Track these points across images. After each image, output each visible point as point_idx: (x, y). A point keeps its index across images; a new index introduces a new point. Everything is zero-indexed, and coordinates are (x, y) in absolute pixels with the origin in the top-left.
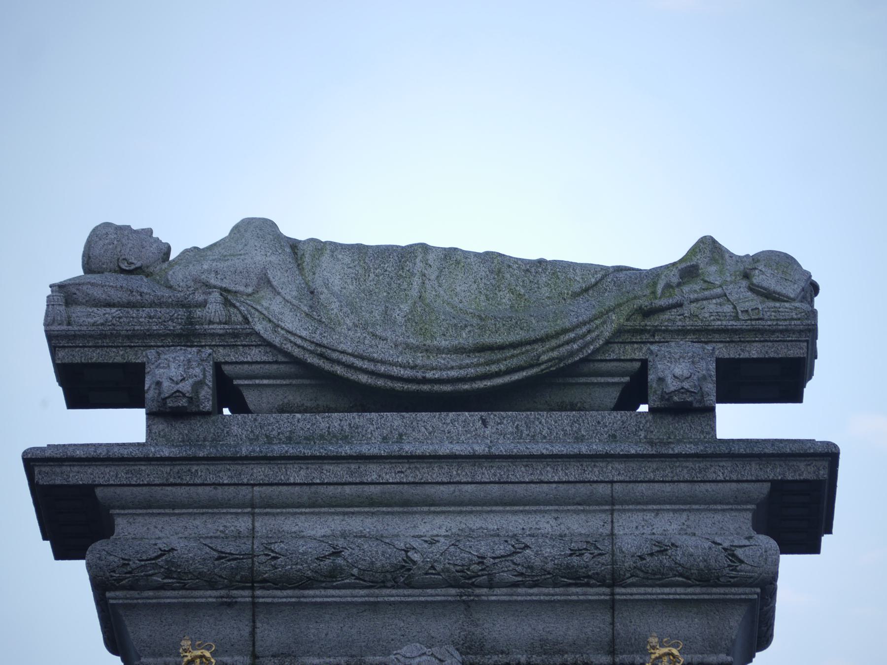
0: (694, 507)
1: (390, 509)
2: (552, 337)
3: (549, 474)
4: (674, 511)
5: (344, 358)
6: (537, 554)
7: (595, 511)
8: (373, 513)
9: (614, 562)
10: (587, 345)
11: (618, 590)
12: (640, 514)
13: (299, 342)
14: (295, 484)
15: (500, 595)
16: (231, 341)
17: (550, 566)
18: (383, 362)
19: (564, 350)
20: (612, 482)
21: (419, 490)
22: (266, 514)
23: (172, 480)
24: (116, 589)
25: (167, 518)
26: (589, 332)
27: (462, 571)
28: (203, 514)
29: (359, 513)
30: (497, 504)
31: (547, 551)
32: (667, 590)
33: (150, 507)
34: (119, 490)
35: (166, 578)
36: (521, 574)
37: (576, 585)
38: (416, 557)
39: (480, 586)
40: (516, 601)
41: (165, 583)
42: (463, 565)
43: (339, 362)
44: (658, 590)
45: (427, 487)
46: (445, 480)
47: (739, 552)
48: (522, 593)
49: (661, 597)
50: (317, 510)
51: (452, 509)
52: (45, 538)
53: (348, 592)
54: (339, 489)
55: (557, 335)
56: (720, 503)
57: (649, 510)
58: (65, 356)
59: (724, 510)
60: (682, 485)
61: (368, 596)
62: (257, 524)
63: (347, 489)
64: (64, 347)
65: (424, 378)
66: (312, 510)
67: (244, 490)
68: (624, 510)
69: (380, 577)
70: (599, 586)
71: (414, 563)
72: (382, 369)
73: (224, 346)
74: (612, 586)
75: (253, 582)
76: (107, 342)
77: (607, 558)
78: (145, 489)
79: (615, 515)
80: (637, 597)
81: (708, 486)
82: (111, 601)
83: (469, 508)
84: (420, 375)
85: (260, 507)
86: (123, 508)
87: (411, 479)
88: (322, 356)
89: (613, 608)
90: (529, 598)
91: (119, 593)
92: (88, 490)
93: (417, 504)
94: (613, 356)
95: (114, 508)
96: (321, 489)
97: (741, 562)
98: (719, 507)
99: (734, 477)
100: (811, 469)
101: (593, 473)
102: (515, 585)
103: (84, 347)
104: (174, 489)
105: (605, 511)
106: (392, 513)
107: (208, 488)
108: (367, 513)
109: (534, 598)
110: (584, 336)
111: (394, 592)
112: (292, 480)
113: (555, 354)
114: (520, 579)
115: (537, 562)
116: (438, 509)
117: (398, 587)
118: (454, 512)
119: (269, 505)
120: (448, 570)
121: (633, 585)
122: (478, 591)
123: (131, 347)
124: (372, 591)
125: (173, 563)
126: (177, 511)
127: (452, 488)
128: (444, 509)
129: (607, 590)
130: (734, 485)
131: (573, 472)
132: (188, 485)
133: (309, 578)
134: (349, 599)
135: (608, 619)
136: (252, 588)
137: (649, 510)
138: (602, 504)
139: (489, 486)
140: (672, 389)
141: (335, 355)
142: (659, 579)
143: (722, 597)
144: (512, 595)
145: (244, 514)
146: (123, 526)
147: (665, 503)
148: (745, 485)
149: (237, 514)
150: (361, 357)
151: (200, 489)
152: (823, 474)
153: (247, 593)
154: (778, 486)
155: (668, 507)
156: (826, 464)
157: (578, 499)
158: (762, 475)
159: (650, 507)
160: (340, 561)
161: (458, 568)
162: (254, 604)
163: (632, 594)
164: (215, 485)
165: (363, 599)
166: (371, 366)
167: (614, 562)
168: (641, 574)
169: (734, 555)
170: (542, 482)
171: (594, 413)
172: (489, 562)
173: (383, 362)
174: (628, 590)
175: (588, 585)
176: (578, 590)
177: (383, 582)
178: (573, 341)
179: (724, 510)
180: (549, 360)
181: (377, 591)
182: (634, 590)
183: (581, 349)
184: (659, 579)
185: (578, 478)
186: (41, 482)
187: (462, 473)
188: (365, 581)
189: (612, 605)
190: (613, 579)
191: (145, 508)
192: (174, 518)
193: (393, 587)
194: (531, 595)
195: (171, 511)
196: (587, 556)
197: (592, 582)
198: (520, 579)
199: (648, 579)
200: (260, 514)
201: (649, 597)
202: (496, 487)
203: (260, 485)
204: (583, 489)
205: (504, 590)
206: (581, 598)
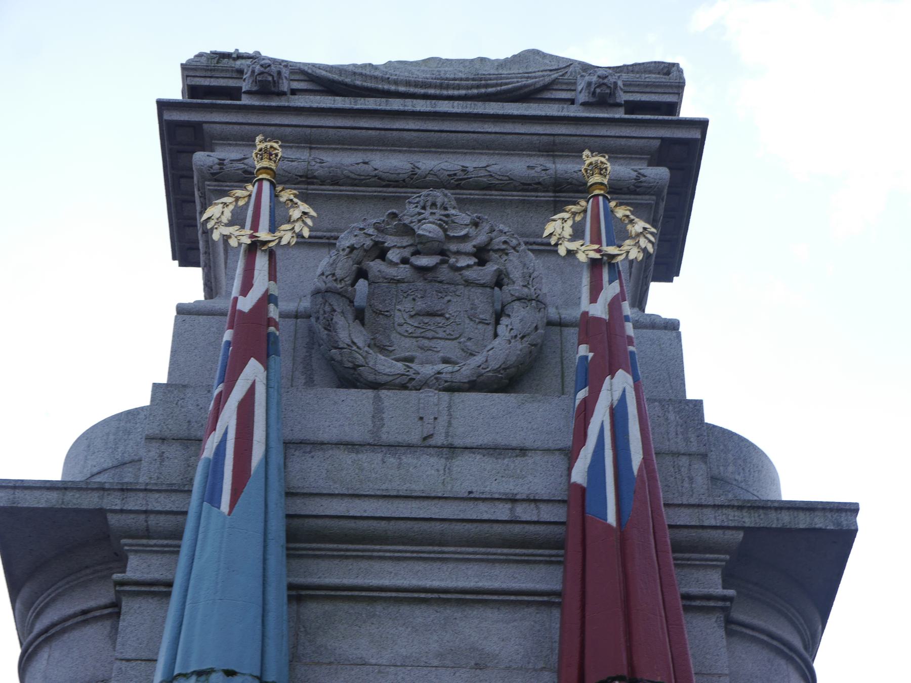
154: (666, 142)
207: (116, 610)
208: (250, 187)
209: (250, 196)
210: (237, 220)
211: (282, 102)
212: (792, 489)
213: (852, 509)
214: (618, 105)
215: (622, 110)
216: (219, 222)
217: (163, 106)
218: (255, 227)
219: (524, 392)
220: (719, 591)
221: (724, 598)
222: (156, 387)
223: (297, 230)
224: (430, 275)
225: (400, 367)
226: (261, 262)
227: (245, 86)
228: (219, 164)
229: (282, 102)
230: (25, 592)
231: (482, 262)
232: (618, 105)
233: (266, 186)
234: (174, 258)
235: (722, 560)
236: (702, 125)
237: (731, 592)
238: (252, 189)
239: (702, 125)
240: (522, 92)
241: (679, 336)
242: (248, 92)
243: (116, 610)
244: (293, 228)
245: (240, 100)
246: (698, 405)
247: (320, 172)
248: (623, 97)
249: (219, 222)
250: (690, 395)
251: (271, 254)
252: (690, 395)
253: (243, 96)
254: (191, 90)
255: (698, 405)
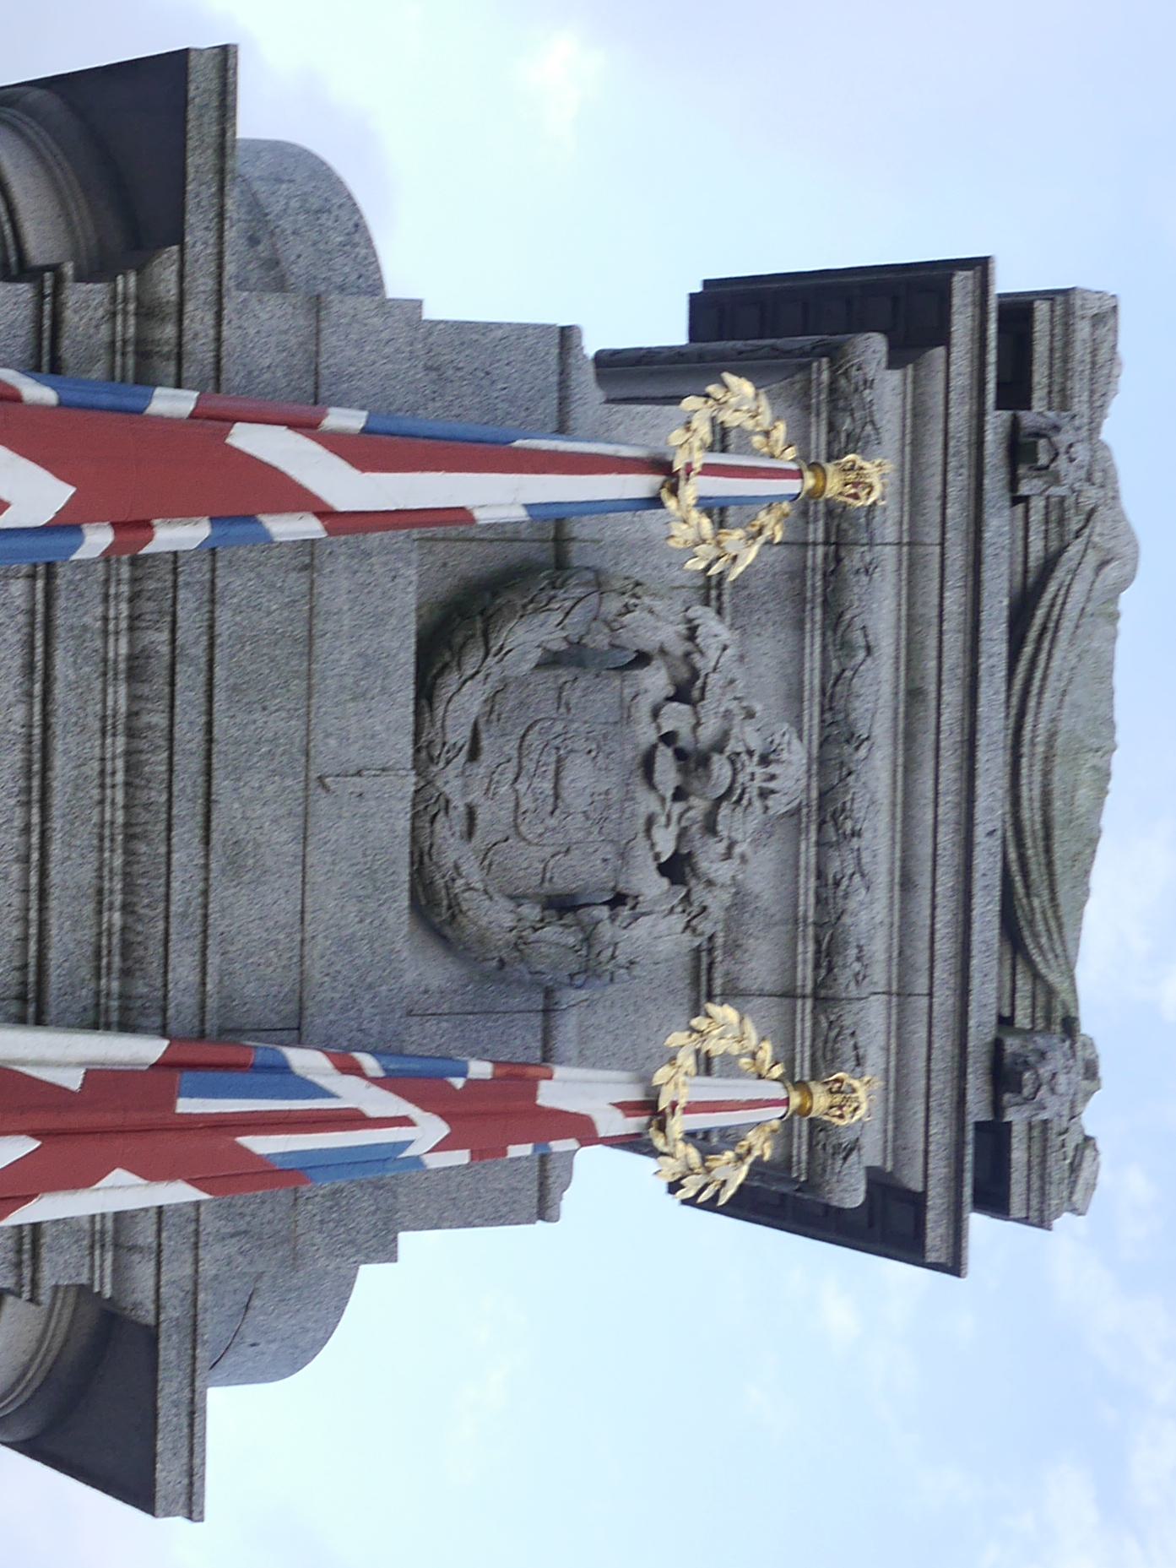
0: (892, 1095)
1: (901, 716)
2: (1055, 912)
3: (944, 917)
4: (887, 1070)
5: (1043, 656)
6: (862, 904)
7: (889, 971)
8: (896, 694)
9: (850, 1000)
10: (1042, 953)
11: (809, 1003)
12: (883, 1028)
13: (1060, 600)
14: (942, 598)
15: (808, 853)
16: (1054, 517)
17: (847, 920)
18: (1039, 703)
19: (1041, 927)
20: (931, 995)
21: (929, 755)
22: (900, 561)
23: (952, 443)
24: (833, 372)
25: (898, 437)
26: (1056, 956)
27: (843, 810)
28: (902, 480)
29: (898, 678)
30: (904, 851)
31: (864, 916)
32: (807, 1065)
33: (915, 416)
34: (941, 376)
35: (848, 436)
36: (837, 884)
37: (818, 952)
38: (863, 752)
39: (820, 830)
40: (797, 876)
41: (838, 433)
42: (852, 810)
43: (1037, 651)
44: (807, 1054)
45: (932, 763)
46: (940, 787)
47: (854, 1157)
48: (808, 884)
49: (798, 1056)
50: (903, 623)
51: (900, 794)
52: (707, 283)
53: (817, 664)
54: (934, 653)
55: (1058, 918)
56: (896, 1128)
57: (889, 1039)
58: (1042, 309)
59: (885, 1131)
60: (923, 1082)
61: (812, 689)
62: (888, 548)
63: (933, 664)
64: (1052, 311)
65: (1021, 756)
66: (904, 619)
67: (935, 535)
68: (889, 1009)
69: (839, 704)
70: (815, 981)
71: (857, 748)
72: (1032, 703)
73: (1047, 507)
74: (816, 997)
75: (837, 544)
76: (1058, 364)
77: (853, 991)
78: (941, 409)
79: (884, 997)
80: (799, 1027)
81: (921, 1115)
82: (815, 364)
83: (899, 814)
84: (1025, 750)
85: (910, 554)
86: (915, 382)
87: (943, 744)
88: (1044, 629)
89: (784, 995)
90: (802, 891)
91: (825, 376)
92: (942, 337)
93: (907, 750)
94: (1019, 983)
95: (915, 370)
96: (934, 631)
97: (845, 1159)
98: (890, 1126)
99: (932, 1148)
100: (938, 1242)
101: (943, 972)
102: (820, 875)
103: (1052, 336)
104: (940, 445)
105: (889, 985)
106: (895, 718)
107: (939, 488)
108: (897, 687)
109: (802, 898)
110: (1053, 950)
111: (816, 721)
112: (947, 594)
113: (1038, 916)
114: (830, 881)
115: (852, 904)
116: (900, 776)
117: (822, 728)
118: (894, 796)
119: (912, 569)
120: (846, 792)
121: (816, 1023)
122: (813, 827)
123: (1050, 392)
124: (817, 693)
125: (867, 443)
126: (908, 449)
127: (930, 795)
128: (900, 783)
129: (809, 989)
130: (921, 1146)
131: (945, 947)
132: (946, 463)
133: (841, 615)
134: (807, 665)
135: (768, 988)
136: (826, 543)
137: (889, 1039)
138: (899, 981)
139: (930, 841)
140: (1041, 1071)
141: (1046, 645)
142: (824, 1056)
143: (796, 1133)
144: (807, 869)
145: (901, 532)
146: (894, 377)
147: (899, 1060)
148: (920, 1160)
149: (901, 523)
150: (1044, 678)
151: (938, 479)
152: (932, 1257)
153: (820, 536)
154: (918, 1201)
155: (893, 1064)
156: (942, 1260)
157: (908, 952)
158: (932, 1182)
159: (893, 1041)
160: (861, 654)
161: (848, 805)
162: (805, 544)
163: (803, 1020)
164: (944, 496)
165: (807, 682)
166: (1035, 690)
167: (850, 1000)
168: (833, 1034)
169: (852, 1150)
170: (934, 907)
171: (996, 970)
172: (855, 843)
173: (1039, 703)
174: (808, 1017)
175: (817, 966)
176: (810, 955)
177: (831, 709)
178: (1050, 938)
179: (885, 1131)
180: (1032, 909)
181: (817, 700)
182: (808, 1024)
183: (1040, 947)
184: (824, 1056)
185: (937, 953)
186: (955, 279)
187: (949, 810)
188: (835, 684)
189: (789, 994)
190: (826, 999)
191: (914, 408)
192: (897, 445)
193: (823, 721)
194: (806, 894)
195: (908, 441)
196: (857, 966)
197: (823, 972)
198: (830, 881)
199: (826, 1042)
200: (900, 554)
201: (799, 1042)
202: (929, 850)
203: (943, 554)
204: (922, 959)
205: (813, 861)
206: (800, 958)
207: (14, 272)
208: (791, 453)
209: (772, 456)
210: (722, 437)
211: (995, 482)
212: (226, 1407)
213: (192, 1509)
214: (997, 1108)
215: (985, 1116)
216: (721, 404)
217: (981, 266)
218: (709, 470)
219: (1001, 941)
220: (48, 1279)
221: (35, 1284)
222: (418, 304)
223: (701, 549)
224: (638, 779)
225: (459, 735)
226: (639, 485)
227: (1028, 419)
228: (865, 382)
229: (995, 482)
230: (50, 102)
231: (665, 869)
232: (997, 1108)
233: (792, 486)
234: (707, 283)
235: (102, 1285)
236: (954, 1266)
237: (45, 1297)
238: (788, 459)
239: (954, 1266)
240: (1026, 933)
241: (530, 1221)
242: (1015, 423)
243: (14, 272)
244: (704, 541)
245: (998, 407)
246: (388, 1252)
247: (854, 559)
248: (1016, 1117)
249: (721, 404)
250: (406, 1239)
251: (655, 502)
252: (406, 1239)
253: (1006, 415)
254: (1017, 313)
255: (388, 1252)
